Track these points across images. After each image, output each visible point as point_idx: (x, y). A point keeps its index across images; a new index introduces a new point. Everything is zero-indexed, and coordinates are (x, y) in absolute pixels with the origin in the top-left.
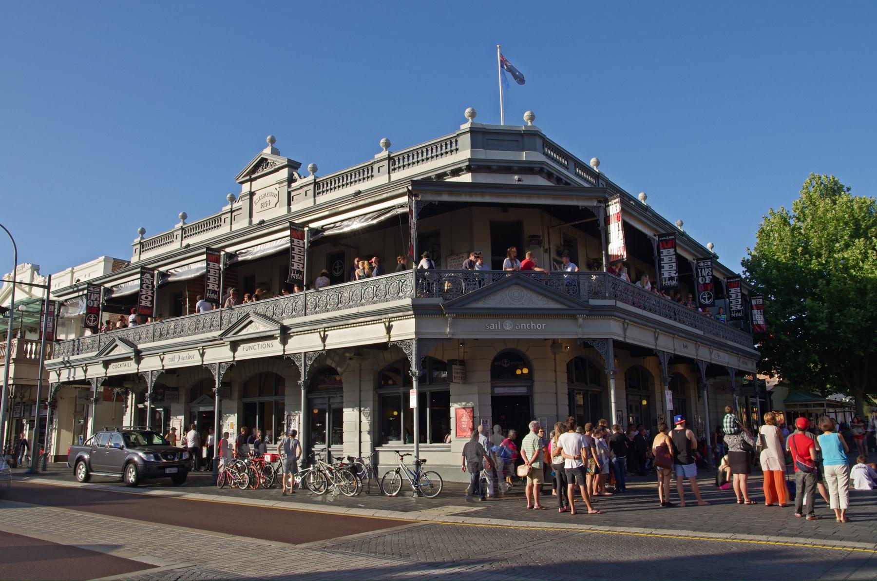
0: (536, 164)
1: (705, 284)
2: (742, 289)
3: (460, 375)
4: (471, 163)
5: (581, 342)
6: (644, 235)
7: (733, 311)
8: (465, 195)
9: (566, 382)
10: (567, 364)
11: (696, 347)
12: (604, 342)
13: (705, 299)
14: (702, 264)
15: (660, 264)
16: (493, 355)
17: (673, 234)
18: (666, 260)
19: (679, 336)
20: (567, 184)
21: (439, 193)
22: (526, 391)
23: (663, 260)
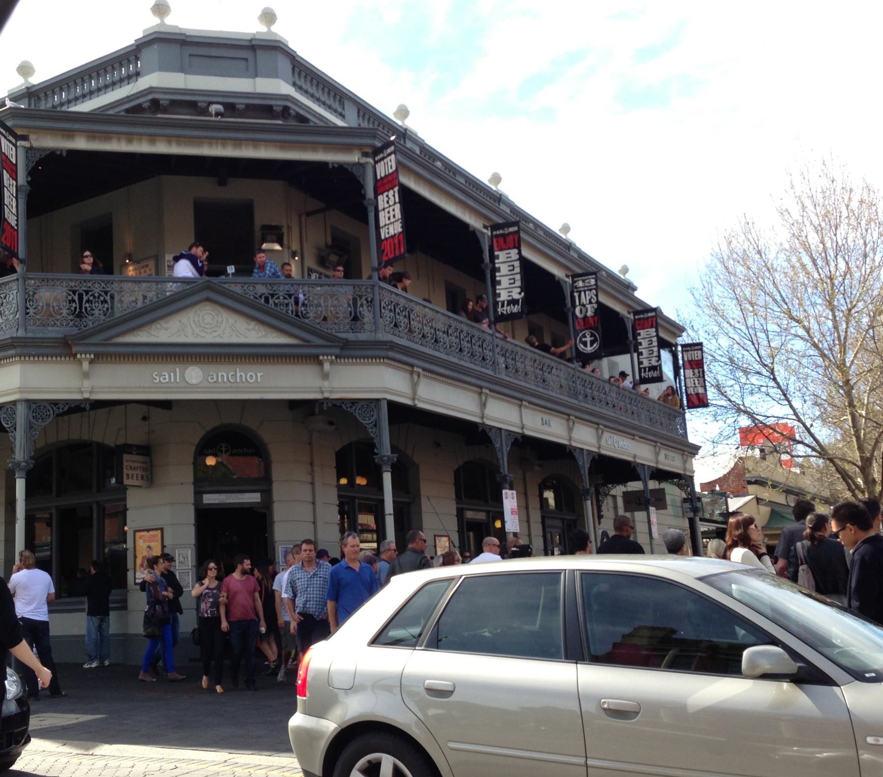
1: (585, 318)
2: (660, 329)
3: (139, 472)
5: (330, 405)
6: (616, 314)
7: (645, 368)
10: (455, 472)
11: (568, 425)
12: (373, 405)
13: (585, 344)
14: (580, 284)
15: (493, 277)
17: (516, 224)
18: (504, 269)
19: (530, 403)
20: (303, 120)
21: (69, 134)
22: (259, 500)
23: (499, 270)
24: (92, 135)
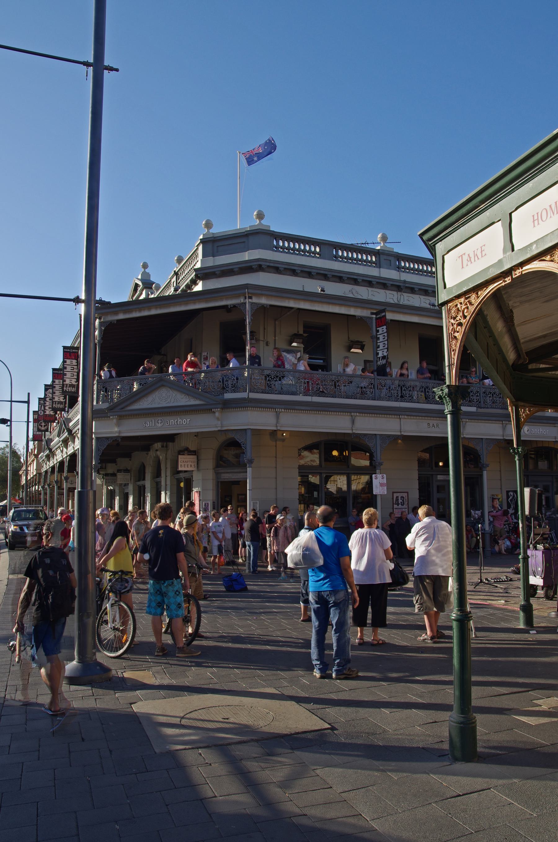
0: (253, 262)
4: (197, 273)
8: (136, 311)
9: (417, 468)
16: (216, 444)
21: (116, 313)
24: (125, 312)
